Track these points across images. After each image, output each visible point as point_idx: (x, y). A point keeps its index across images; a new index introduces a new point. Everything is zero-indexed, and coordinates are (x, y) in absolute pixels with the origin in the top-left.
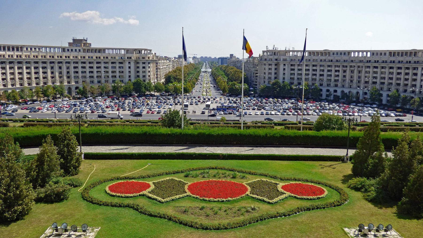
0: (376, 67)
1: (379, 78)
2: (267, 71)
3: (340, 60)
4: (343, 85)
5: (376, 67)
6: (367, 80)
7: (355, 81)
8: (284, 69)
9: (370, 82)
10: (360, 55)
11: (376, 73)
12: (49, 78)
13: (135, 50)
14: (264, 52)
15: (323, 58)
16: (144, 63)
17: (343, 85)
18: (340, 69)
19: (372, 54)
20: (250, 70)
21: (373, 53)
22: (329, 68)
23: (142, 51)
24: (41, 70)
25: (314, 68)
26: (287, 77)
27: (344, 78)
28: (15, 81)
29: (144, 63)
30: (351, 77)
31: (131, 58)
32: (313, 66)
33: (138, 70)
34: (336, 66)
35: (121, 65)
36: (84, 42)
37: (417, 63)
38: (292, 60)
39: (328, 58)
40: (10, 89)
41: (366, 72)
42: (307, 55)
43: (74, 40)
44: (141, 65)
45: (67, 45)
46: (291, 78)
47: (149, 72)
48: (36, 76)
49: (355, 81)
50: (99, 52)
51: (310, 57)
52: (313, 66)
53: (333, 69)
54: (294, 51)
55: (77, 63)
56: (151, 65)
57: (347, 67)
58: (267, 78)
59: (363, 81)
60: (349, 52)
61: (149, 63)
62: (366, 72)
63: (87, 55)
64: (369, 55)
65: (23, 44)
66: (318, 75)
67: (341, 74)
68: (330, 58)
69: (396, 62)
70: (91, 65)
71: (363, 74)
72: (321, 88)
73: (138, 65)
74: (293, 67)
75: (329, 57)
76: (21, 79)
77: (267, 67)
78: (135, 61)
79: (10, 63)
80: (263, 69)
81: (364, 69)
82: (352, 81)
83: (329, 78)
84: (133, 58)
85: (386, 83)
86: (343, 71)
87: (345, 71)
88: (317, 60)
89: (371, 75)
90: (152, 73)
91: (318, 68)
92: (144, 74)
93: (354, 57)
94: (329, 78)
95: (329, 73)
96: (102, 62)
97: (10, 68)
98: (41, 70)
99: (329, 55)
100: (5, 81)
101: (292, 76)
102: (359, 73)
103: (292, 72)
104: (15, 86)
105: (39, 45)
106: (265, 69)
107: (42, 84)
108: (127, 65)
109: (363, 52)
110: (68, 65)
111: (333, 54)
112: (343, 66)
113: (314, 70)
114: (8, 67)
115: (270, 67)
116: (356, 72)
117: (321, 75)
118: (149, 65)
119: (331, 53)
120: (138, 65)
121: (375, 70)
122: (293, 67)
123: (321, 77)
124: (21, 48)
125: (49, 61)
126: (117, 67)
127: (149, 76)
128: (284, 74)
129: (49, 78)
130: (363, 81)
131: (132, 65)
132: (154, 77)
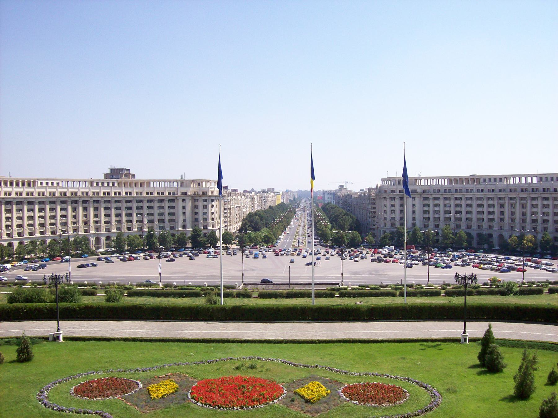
0: (547, 199)
1: (551, 214)
2: (388, 209)
3: (494, 190)
4: (501, 227)
5: (547, 199)
6: (535, 218)
7: (517, 221)
8: (414, 205)
9: (540, 221)
10: (523, 182)
11: (547, 206)
12: (70, 225)
13: (193, 181)
14: (383, 180)
15: (470, 187)
16: (205, 200)
17: (501, 227)
18: (496, 202)
19: (539, 180)
20: (365, 207)
21: (541, 178)
22: (480, 202)
23: (202, 182)
24: (113, 212)
25: (458, 202)
26: (419, 216)
27: (502, 216)
28: (67, 226)
29: (205, 200)
30: (512, 215)
31: (186, 193)
32: (456, 199)
33: (197, 210)
34: (467, 199)
35: (172, 204)
36: (126, 172)
37: (536, 191)
38: (424, 191)
39: (475, 186)
40: (16, 240)
41: (533, 206)
42: (446, 184)
43: (111, 170)
44: (201, 204)
45: (103, 177)
46: (424, 218)
47: (213, 213)
48: (107, 220)
49: (517, 221)
50: (141, 186)
51: (450, 186)
52: (456, 199)
53: (485, 203)
54: (427, 179)
55: (109, 202)
56: (215, 203)
57: (394, 199)
58: (388, 218)
59: (529, 221)
60: (507, 177)
61: (213, 200)
62: (533, 206)
64: (535, 181)
65: (37, 178)
66: (464, 213)
67: (496, 209)
68: (480, 187)
69: (507, 190)
70: (129, 205)
71: (528, 210)
72: (490, 231)
73: (197, 204)
74: (426, 202)
75: (478, 186)
76: (119, 222)
77: (388, 203)
78: (192, 197)
79: (40, 203)
80: (383, 205)
81: (529, 202)
82: (513, 220)
83: (480, 216)
84: (188, 194)
85: (551, 221)
86: (499, 206)
87: (502, 206)
88: (461, 191)
89: (539, 210)
90: (216, 216)
91: (463, 202)
92: (205, 217)
93: (515, 184)
94: (480, 216)
95: (480, 209)
96: (124, 200)
97: (40, 210)
98: (113, 212)
99: (478, 183)
100: (10, 228)
101: (426, 216)
102: (523, 207)
103: (426, 209)
104: (68, 232)
105: (58, 178)
106: (385, 206)
107: (59, 232)
108: (181, 204)
109: (526, 176)
110: (96, 205)
111: (485, 180)
112: (500, 198)
113: (457, 205)
114: (59, 208)
115: (393, 202)
116: (506, 206)
117: (468, 212)
118: (213, 203)
119: (482, 180)
120: (197, 204)
121: (546, 202)
122: (426, 202)
123: (469, 216)
124: (34, 182)
125: (156, 200)
126: (166, 207)
127: (213, 219)
128: (414, 212)
129: (70, 225)
130: (529, 221)
131: (189, 205)
132: (224, 220)
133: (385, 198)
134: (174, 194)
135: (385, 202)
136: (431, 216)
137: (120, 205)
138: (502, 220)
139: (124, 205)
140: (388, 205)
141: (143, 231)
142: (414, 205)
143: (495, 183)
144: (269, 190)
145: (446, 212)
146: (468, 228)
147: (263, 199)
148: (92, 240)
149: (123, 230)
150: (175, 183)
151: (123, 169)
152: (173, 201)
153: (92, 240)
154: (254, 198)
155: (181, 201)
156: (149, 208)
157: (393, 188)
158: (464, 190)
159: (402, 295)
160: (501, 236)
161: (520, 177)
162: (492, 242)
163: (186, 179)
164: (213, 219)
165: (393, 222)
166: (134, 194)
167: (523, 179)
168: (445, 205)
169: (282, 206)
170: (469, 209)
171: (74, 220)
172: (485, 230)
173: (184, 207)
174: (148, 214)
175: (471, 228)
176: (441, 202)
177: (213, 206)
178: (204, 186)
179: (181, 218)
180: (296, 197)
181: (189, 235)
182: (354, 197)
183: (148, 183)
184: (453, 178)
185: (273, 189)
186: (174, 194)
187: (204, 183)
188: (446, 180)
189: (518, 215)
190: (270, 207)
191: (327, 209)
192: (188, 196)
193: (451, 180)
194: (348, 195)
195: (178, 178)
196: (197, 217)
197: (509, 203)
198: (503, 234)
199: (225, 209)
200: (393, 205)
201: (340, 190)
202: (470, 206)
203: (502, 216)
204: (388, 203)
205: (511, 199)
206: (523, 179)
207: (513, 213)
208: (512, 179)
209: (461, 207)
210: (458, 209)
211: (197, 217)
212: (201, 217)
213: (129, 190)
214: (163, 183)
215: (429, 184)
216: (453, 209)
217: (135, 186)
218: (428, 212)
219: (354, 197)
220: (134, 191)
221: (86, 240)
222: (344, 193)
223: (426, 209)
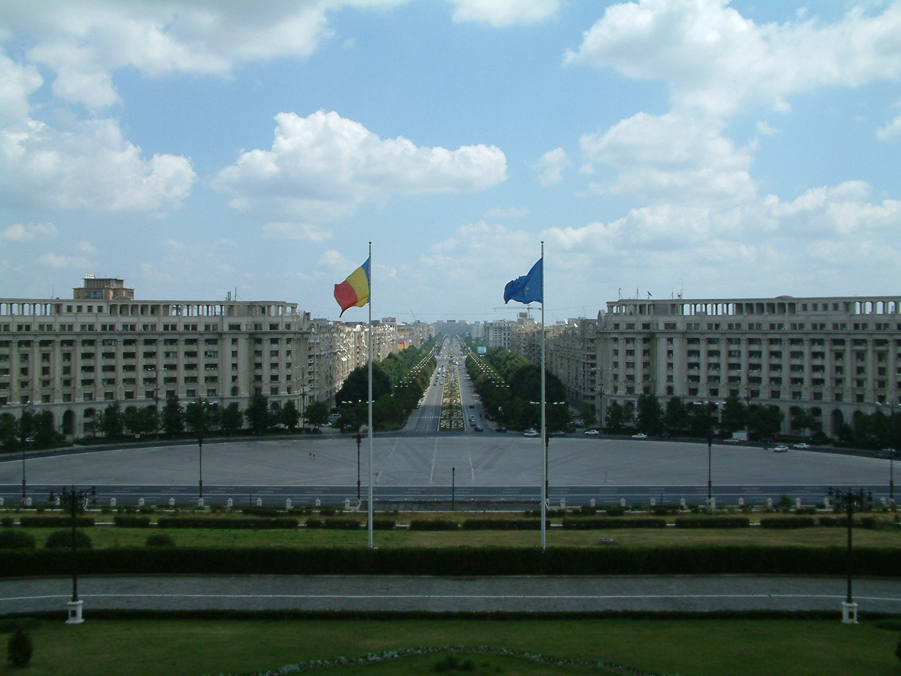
8: (670, 352)
14: (610, 305)
15: (776, 318)
18: (826, 349)
21: (743, 306)
22: (796, 348)
23: (269, 307)
25: (754, 348)
27: (839, 376)
29: (274, 341)
33: (258, 360)
36: (115, 286)
42: (730, 313)
50: (152, 313)
63: (119, 321)
73: (259, 347)
74: (693, 347)
80: (611, 352)
86: (834, 356)
90: (295, 370)
95: (796, 362)
101: (693, 372)
103: (693, 360)
106: (616, 352)
115: (630, 347)
120: (259, 347)
122: (693, 347)
127: (289, 377)
128: (670, 365)
133: (616, 340)
134: (215, 326)
135: (615, 346)
136: (703, 373)
137: (112, 349)
138: (860, 383)
139: (786, 349)
140: (622, 353)
141: (157, 400)
142: (670, 352)
143: (825, 313)
144: (386, 320)
145: (732, 366)
146: (773, 397)
147: (375, 342)
148: (58, 421)
149: (119, 398)
150: (218, 308)
151: (110, 280)
152: (213, 342)
153: (58, 421)
154: (360, 337)
155: (228, 341)
156: (127, 355)
157: (632, 319)
158: (768, 322)
159: (312, 525)
160: (837, 415)
161: (873, 301)
162: (820, 424)
163: (238, 300)
164: (289, 377)
165: (630, 384)
166: (139, 328)
167: (880, 305)
168: (730, 354)
169: (411, 355)
170: (775, 361)
171: (24, 378)
172: (806, 403)
173: (234, 354)
174: (165, 366)
175: (778, 397)
176: (723, 348)
177: (289, 353)
178: (273, 313)
179: (229, 373)
180: (433, 335)
181: (244, 406)
182: (550, 335)
183: (166, 306)
184: (744, 303)
185: (394, 320)
186: (215, 326)
187: (273, 307)
188: (730, 306)
189: (870, 374)
190: (391, 356)
191: (499, 360)
192: (243, 333)
193: (740, 306)
194: (539, 332)
195: (223, 299)
196: (258, 372)
197: (852, 351)
198: (842, 409)
199: (310, 357)
200: (631, 353)
201: (521, 322)
202: (777, 354)
203: (839, 376)
204: (622, 347)
205: (857, 342)
206: (880, 305)
207: (860, 370)
208: (858, 304)
209: (739, 356)
210: (755, 361)
211: (258, 372)
212: (266, 373)
213: (129, 320)
214: (205, 307)
215: (720, 313)
216: (744, 361)
217: (142, 313)
218: (698, 365)
219: (550, 335)
220: (139, 321)
221: (48, 417)
222: (527, 328)
223: (693, 360)
